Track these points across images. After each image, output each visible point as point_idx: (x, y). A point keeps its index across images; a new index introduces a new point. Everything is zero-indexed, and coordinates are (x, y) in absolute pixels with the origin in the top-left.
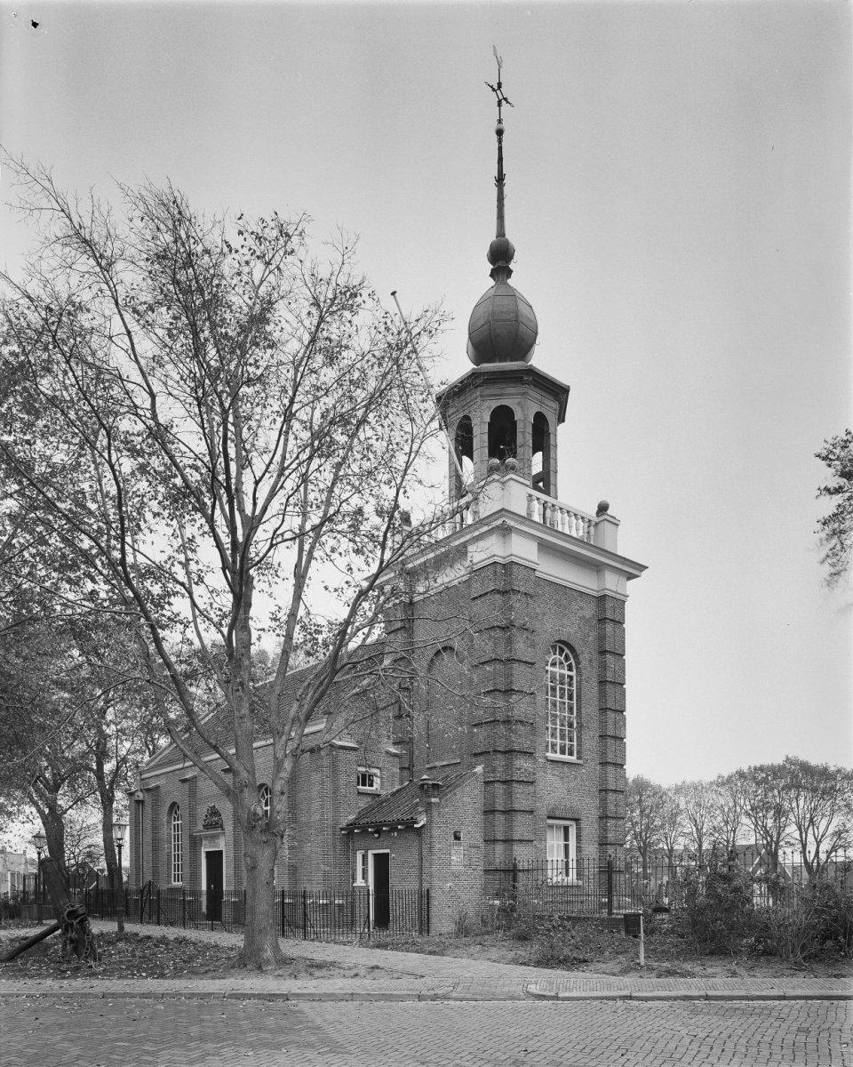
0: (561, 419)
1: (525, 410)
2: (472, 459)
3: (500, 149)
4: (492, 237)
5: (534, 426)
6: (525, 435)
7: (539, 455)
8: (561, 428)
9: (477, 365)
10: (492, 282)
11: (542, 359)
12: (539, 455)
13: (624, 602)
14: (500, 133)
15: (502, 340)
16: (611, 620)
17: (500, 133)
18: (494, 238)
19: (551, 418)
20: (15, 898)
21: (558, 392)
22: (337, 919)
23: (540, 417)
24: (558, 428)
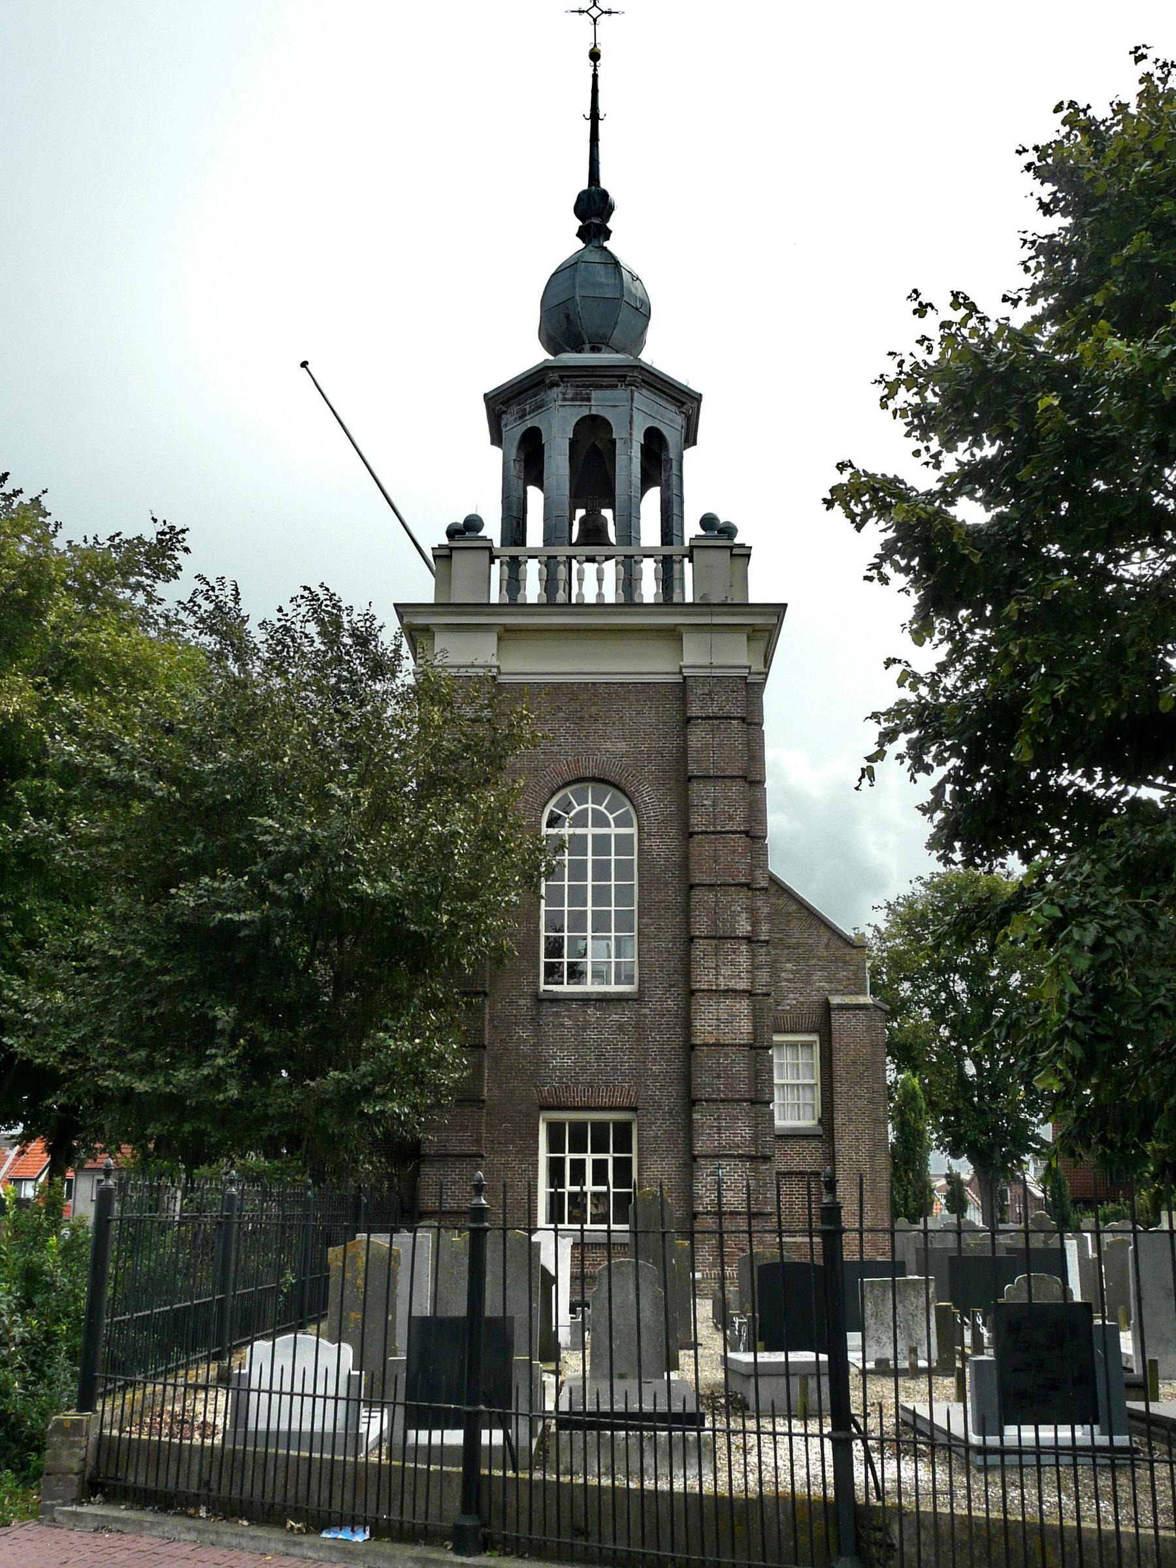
0: (690, 439)
1: (632, 419)
2: (541, 487)
3: (595, 77)
4: (584, 185)
5: (645, 449)
6: (629, 462)
7: (654, 495)
8: (688, 454)
9: (554, 355)
10: (580, 245)
11: (660, 352)
12: (654, 495)
13: (751, 688)
14: (595, 56)
15: (591, 308)
16: (703, 719)
17: (595, 56)
18: (586, 187)
19: (672, 436)
20: (945, 1150)
21: (686, 402)
22: (211, 1408)
23: (654, 438)
24: (686, 453)
